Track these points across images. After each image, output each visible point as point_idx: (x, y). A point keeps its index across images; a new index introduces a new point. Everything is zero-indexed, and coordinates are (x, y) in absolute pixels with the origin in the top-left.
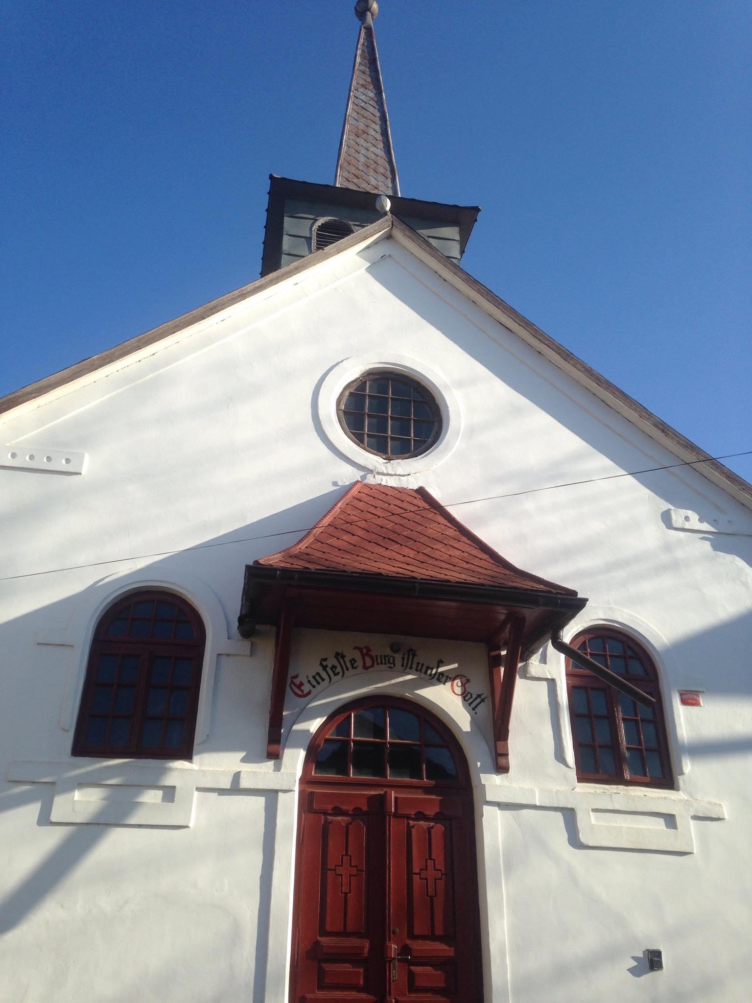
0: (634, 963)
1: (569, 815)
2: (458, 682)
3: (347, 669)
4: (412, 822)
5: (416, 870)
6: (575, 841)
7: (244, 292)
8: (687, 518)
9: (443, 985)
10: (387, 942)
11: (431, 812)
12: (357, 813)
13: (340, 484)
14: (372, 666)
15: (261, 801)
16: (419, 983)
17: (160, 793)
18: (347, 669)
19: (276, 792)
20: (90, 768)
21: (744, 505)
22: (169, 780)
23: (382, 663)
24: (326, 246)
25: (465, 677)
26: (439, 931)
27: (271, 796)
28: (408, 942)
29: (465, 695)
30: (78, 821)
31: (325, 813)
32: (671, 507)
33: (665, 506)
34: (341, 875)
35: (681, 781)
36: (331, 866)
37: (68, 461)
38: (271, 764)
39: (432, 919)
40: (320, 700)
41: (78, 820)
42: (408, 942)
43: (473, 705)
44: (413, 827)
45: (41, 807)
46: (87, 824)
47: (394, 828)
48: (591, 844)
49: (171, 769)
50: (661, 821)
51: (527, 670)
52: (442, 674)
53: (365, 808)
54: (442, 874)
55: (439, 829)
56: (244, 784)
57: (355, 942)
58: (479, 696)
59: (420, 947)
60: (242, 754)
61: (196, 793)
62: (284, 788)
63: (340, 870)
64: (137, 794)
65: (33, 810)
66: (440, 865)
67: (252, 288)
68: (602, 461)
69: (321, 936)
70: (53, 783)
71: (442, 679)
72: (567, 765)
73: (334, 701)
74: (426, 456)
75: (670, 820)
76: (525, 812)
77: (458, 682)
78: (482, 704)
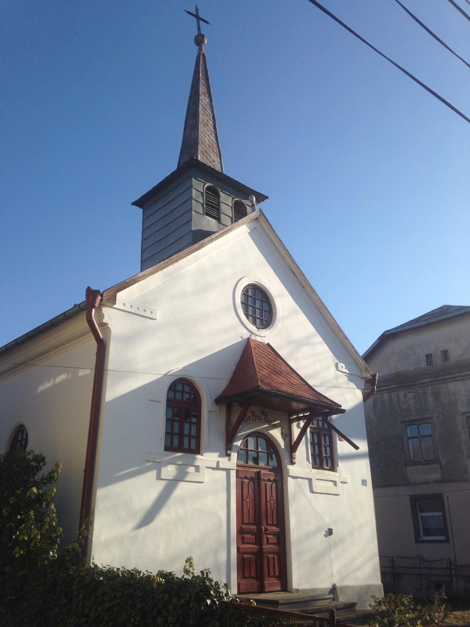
0: (325, 533)
1: (310, 480)
2: (280, 428)
3: (248, 421)
4: (266, 483)
5: (268, 501)
6: (312, 491)
7: (212, 238)
8: (342, 367)
9: (276, 542)
10: (295, 528)
11: (272, 478)
12: (252, 479)
13: (243, 338)
14: (255, 420)
15: (225, 473)
16: (270, 541)
17: (194, 468)
18: (248, 421)
19: (230, 469)
20: (172, 457)
21: (357, 363)
22: (197, 463)
23: (258, 419)
24: (240, 219)
25: (282, 426)
26: (275, 523)
27: (228, 471)
28: (266, 527)
29: (282, 434)
30: (170, 479)
31: (242, 478)
32: (338, 362)
33: (337, 361)
34: (247, 502)
35: (339, 469)
36: (244, 499)
37: (151, 312)
38: (227, 458)
39: (273, 518)
40: (241, 433)
41: (170, 478)
42: (266, 527)
43: (285, 438)
44: (267, 484)
45: (157, 472)
46: (173, 480)
47: (263, 484)
48: (316, 492)
49: (197, 459)
50: (332, 483)
51: (299, 425)
52: (275, 424)
53: (254, 477)
54: (245, 500)
55: (274, 485)
56: (221, 466)
57: (251, 527)
58: (286, 434)
59: (269, 528)
60: (218, 454)
61: (206, 469)
62: (233, 468)
63: (247, 500)
64: (187, 468)
65: (154, 473)
66: (275, 499)
67: (214, 237)
68: (319, 339)
69: (243, 525)
70: (160, 462)
71: (275, 427)
72: (310, 463)
73: (243, 434)
74: (270, 329)
75: (335, 483)
76: (299, 479)
77: (280, 428)
78: (287, 437)
